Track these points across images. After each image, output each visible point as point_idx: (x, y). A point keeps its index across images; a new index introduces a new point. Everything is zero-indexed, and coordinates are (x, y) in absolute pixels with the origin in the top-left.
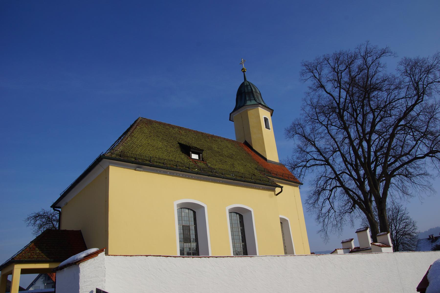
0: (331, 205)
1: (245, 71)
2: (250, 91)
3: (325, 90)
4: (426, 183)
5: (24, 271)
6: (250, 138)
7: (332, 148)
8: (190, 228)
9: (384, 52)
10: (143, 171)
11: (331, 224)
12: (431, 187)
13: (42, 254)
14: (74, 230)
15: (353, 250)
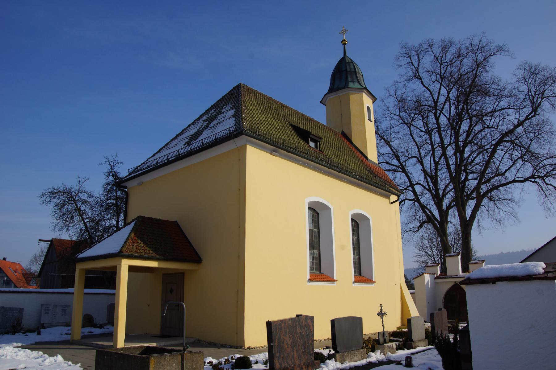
1: (346, 44)
2: (353, 70)
3: (422, 83)
4: (510, 210)
5: (132, 269)
9: (500, 50)
12: (515, 215)
13: (148, 248)
14: (162, 218)
15: (439, 276)
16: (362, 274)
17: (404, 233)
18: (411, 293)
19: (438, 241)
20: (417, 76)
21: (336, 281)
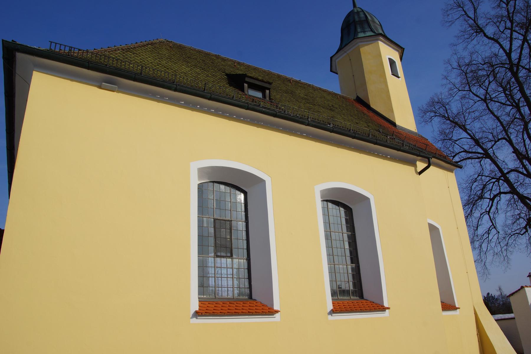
0: (492, 222)
2: (364, 19)
3: (485, 35)
6: (366, 91)
7: (490, 137)
8: (233, 225)
10: (118, 92)
11: (491, 251)
16: (364, 296)
17: (508, 238)
18: (496, 320)
20: (479, 30)
21: (459, 308)
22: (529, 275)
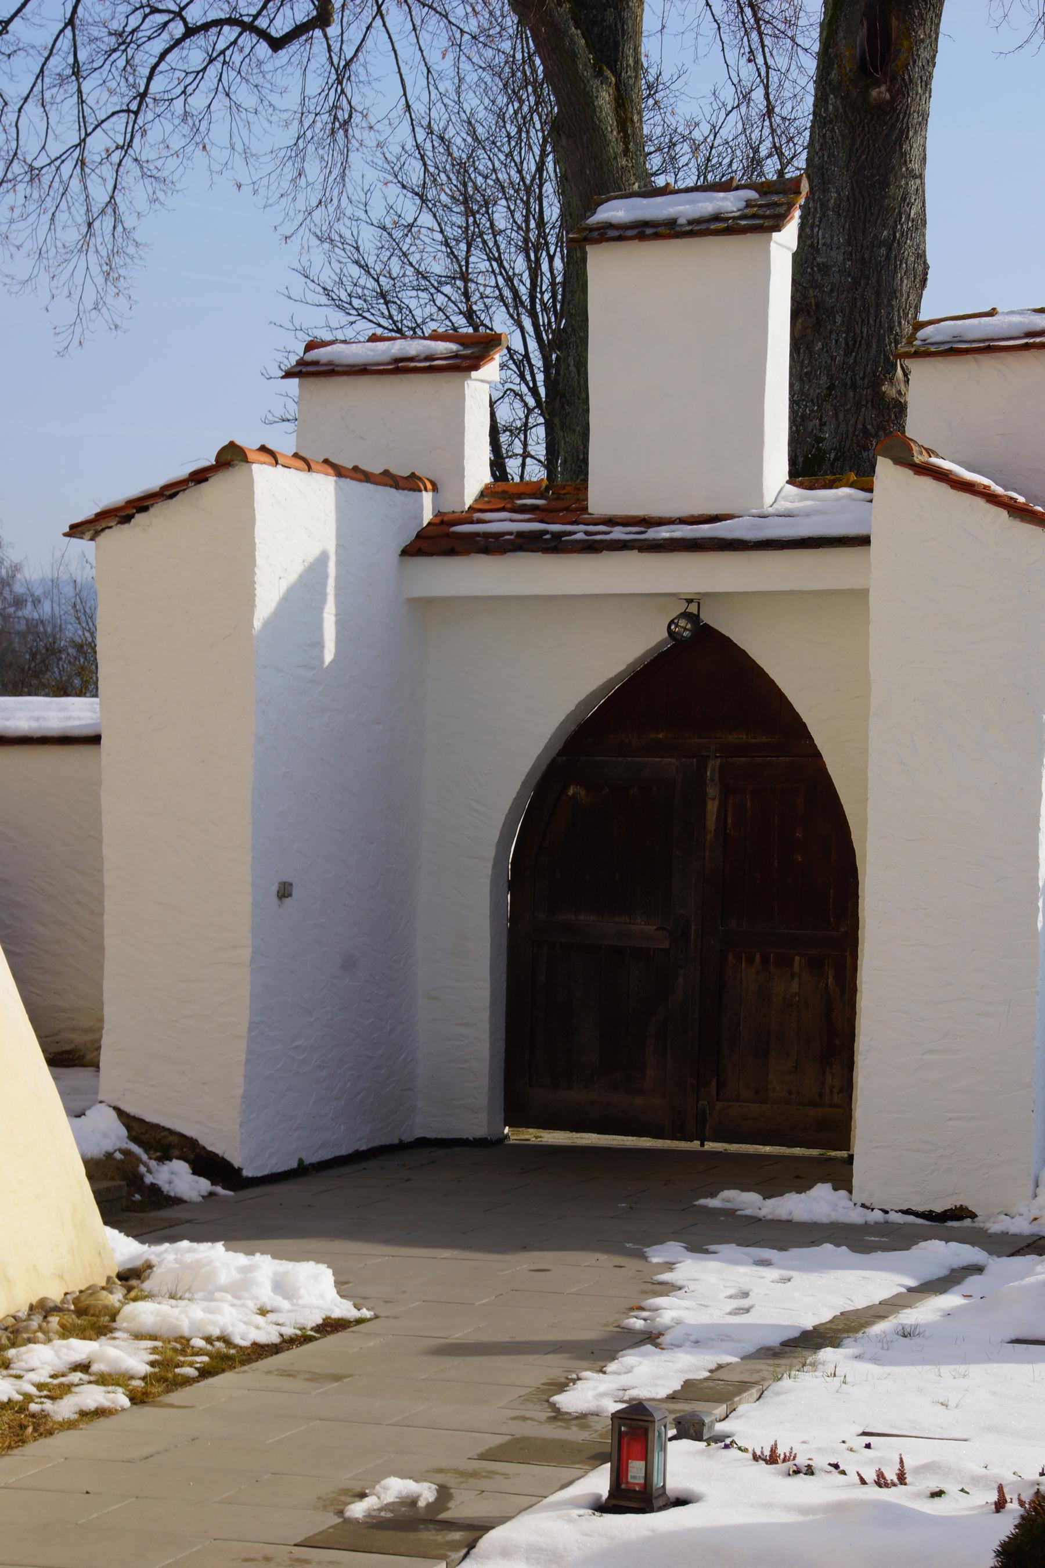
17: (158, 46)
19: (541, 223)
22: (301, 363)
